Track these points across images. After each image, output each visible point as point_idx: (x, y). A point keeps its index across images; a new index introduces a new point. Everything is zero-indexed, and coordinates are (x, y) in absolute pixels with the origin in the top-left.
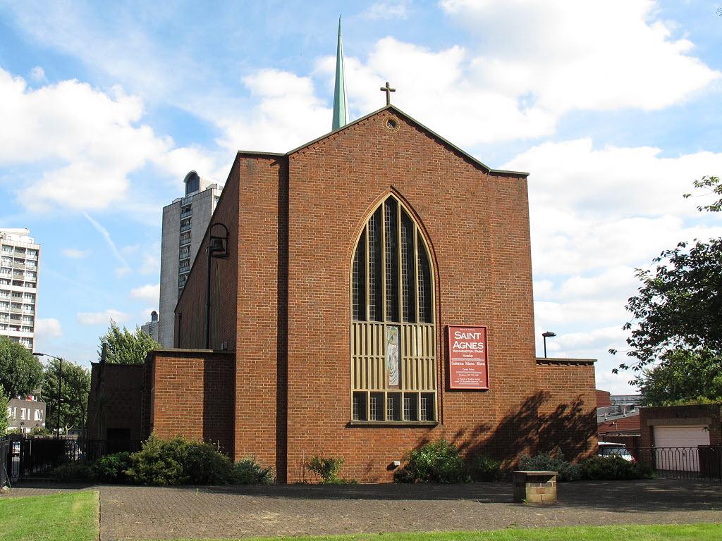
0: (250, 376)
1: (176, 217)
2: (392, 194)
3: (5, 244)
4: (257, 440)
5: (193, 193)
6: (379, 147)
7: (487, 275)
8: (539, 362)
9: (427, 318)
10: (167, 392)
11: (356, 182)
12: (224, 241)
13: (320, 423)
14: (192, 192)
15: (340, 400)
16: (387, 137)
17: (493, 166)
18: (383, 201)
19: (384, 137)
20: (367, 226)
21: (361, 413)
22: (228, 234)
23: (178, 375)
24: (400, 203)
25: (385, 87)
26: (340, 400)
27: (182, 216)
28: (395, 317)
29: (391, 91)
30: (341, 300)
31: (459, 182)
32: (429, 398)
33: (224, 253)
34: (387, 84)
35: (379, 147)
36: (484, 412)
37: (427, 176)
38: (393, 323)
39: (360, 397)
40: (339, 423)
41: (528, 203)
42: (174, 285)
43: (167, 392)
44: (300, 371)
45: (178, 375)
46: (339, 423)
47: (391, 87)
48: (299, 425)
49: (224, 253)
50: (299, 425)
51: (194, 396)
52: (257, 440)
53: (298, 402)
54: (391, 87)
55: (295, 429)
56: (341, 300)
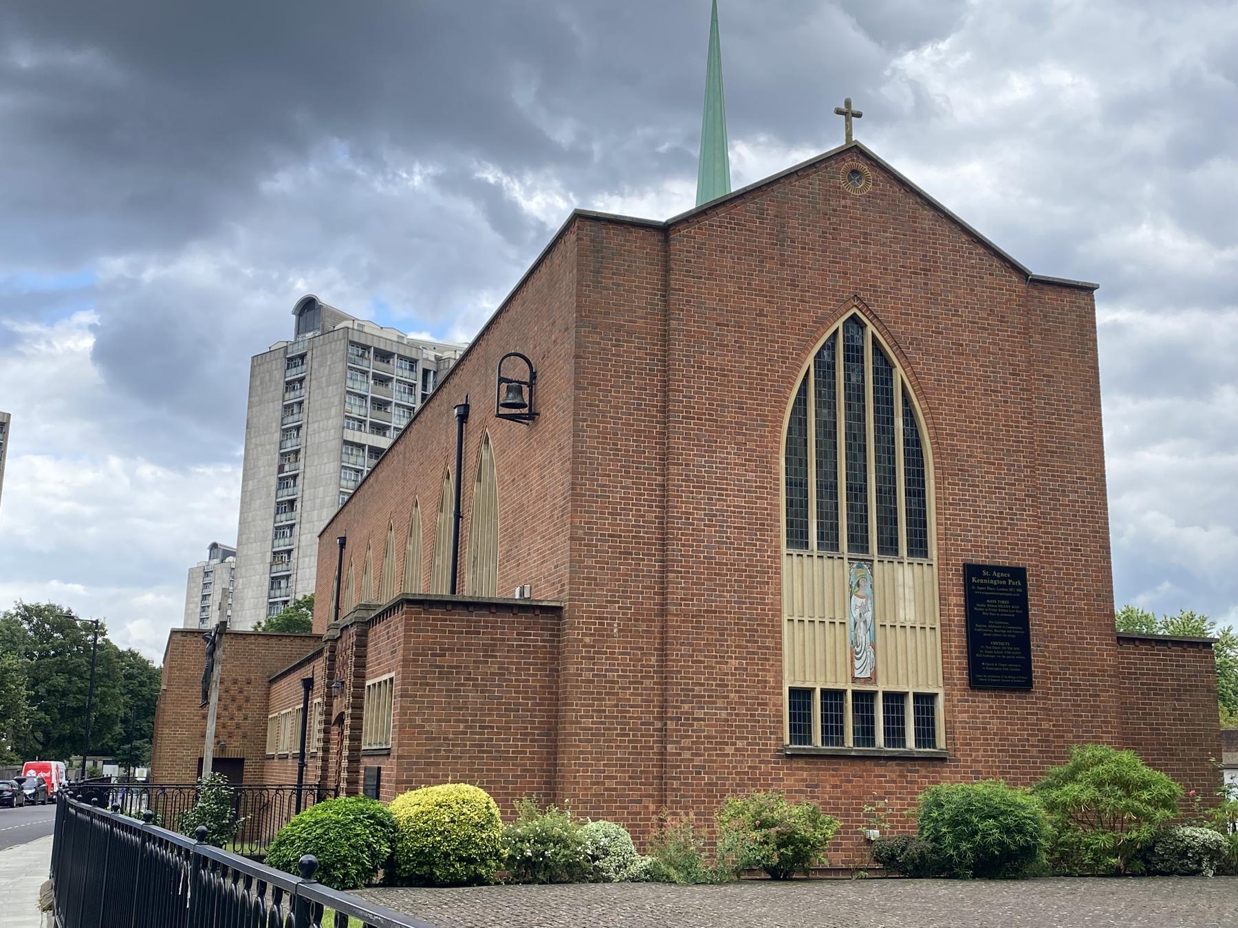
0: (595, 652)
1: (278, 374)
2: (855, 310)
3: (356, 340)
4: (608, 783)
5: (309, 335)
6: (834, 220)
7: (1028, 472)
8: (1123, 640)
9: (918, 547)
10: (427, 684)
11: (793, 285)
12: (526, 389)
13: (729, 750)
14: (306, 332)
15: (766, 704)
16: (849, 202)
17: (1036, 271)
18: (839, 324)
19: (843, 202)
20: (812, 370)
21: (800, 729)
22: (533, 376)
23: (449, 649)
24: (870, 328)
25: (843, 107)
26: (766, 704)
27: (288, 374)
28: (859, 542)
29: (854, 115)
30: (767, 509)
31: (976, 295)
32: (925, 701)
33: (526, 411)
34: (848, 103)
35: (834, 220)
36: (1028, 735)
37: (920, 280)
38: (861, 556)
39: (800, 697)
40: (764, 751)
41: (1095, 340)
42: (269, 495)
43: (427, 684)
44: (690, 645)
45: (449, 649)
46: (764, 751)
47: (855, 108)
48: (687, 755)
49: (526, 411)
50: (687, 755)
51: (482, 692)
52: (608, 783)
53: (686, 707)
54: (854, 108)
55: (682, 761)
56: (767, 509)
